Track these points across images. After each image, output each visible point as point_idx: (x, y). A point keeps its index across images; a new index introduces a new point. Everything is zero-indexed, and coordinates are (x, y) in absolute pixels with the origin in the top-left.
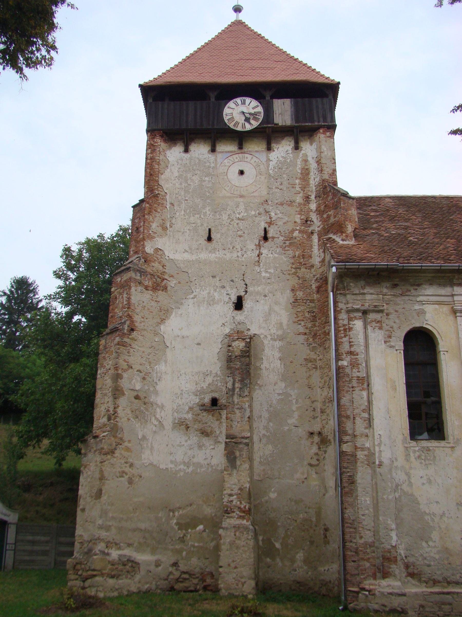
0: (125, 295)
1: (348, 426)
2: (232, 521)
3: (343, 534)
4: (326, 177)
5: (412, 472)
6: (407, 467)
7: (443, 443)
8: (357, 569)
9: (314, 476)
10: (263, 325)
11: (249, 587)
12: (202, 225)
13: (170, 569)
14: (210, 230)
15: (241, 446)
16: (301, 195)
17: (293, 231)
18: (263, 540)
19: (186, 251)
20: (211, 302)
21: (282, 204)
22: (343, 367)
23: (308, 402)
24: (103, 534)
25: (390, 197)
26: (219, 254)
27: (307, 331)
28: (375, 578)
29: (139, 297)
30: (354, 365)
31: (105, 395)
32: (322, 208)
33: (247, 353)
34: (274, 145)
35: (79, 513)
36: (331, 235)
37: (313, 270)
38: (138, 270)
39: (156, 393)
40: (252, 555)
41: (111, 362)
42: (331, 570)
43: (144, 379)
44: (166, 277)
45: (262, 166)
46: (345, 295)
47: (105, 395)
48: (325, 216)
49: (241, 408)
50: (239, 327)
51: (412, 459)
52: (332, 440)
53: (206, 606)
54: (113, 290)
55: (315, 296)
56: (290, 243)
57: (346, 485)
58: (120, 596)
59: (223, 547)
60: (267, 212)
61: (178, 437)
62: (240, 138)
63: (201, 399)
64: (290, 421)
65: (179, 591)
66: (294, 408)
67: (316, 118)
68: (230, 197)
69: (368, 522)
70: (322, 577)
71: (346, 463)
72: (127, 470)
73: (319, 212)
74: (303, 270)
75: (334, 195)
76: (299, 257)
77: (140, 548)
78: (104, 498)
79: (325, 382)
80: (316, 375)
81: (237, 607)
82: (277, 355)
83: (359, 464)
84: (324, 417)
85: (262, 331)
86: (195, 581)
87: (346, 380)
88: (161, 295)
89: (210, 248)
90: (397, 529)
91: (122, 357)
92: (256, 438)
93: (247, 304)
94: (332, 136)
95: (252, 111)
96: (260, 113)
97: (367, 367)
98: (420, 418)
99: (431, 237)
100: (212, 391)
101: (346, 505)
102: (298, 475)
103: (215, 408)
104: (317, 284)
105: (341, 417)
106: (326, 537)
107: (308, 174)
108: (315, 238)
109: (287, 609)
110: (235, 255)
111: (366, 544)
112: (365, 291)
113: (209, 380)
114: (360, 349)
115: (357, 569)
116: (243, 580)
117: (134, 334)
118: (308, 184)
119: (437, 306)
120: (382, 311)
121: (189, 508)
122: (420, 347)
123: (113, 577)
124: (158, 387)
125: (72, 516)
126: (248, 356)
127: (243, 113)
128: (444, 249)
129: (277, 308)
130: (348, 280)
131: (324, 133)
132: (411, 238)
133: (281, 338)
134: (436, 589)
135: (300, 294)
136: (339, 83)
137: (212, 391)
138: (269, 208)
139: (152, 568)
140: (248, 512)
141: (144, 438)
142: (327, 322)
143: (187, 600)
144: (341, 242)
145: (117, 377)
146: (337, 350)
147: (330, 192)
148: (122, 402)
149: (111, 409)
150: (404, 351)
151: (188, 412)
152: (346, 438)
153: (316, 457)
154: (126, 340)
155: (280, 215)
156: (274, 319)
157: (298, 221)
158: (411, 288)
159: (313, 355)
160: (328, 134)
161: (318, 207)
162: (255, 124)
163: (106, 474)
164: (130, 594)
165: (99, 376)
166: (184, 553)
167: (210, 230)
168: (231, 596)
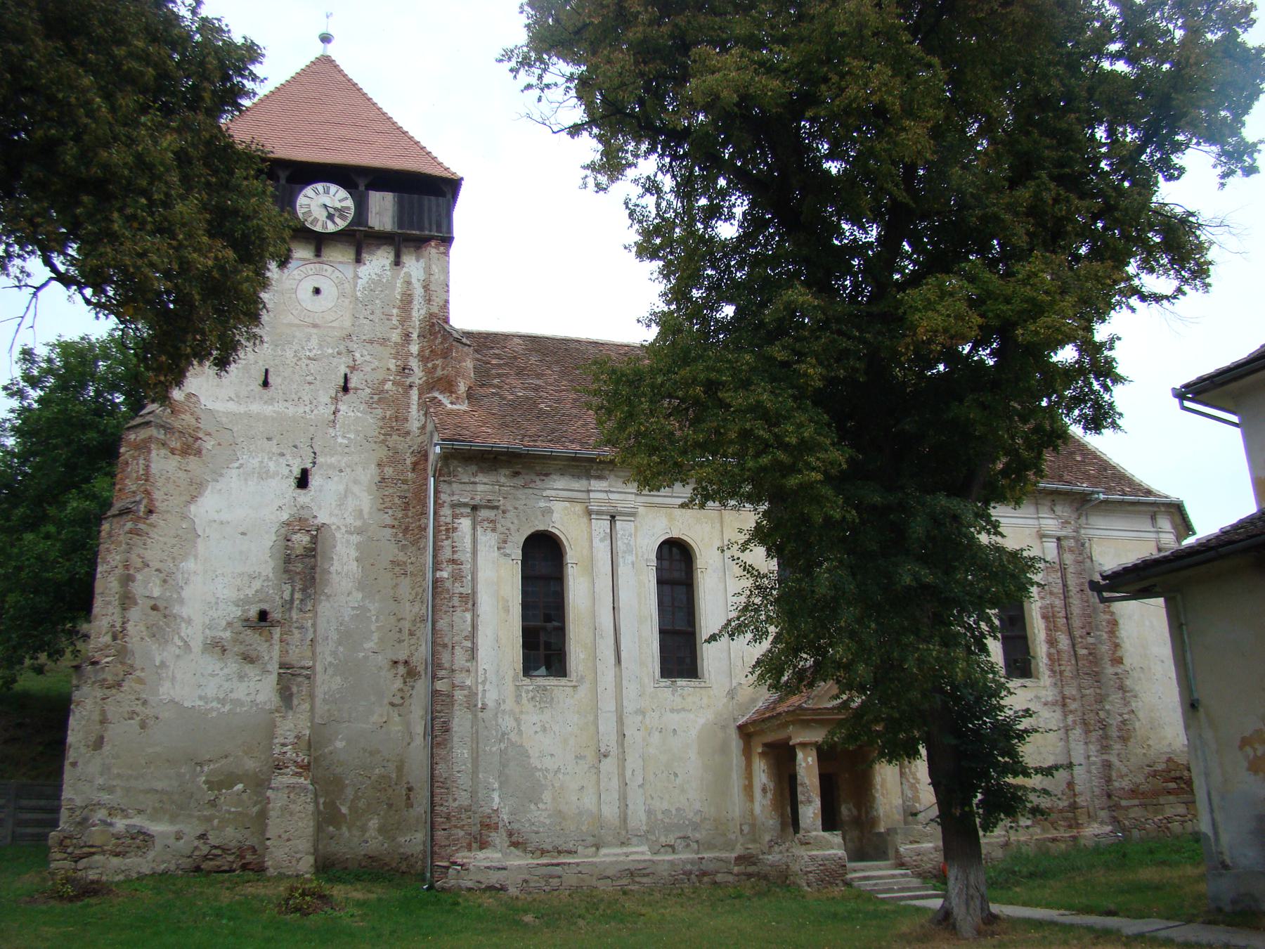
0: (141, 462)
1: (445, 658)
2: (281, 780)
3: (432, 796)
4: (435, 310)
5: (523, 717)
6: (517, 710)
7: (563, 681)
8: (447, 839)
9: (397, 719)
10: (336, 512)
11: (306, 865)
12: (256, 362)
13: (196, 843)
14: (267, 371)
15: (300, 679)
16: (399, 331)
17: (384, 381)
18: (324, 803)
19: (231, 399)
20: (264, 475)
21: (371, 342)
22: (442, 580)
23: (392, 619)
24: (105, 797)
25: (520, 336)
26: (279, 407)
27: (396, 523)
28: (470, 850)
29: (162, 464)
30: (457, 577)
31: (109, 603)
32: (427, 353)
33: (311, 552)
34: (365, 256)
35: (67, 767)
36: (436, 394)
37: (408, 438)
38: (162, 426)
39: (181, 601)
40: (312, 824)
41: (118, 557)
42: (414, 841)
43: (165, 581)
44: (200, 435)
45: (346, 285)
46: (450, 483)
47: (109, 603)
48: (430, 365)
49: (301, 628)
50: (301, 512)
51: (524, 701)
52: (423, 673)
53: (250, 890)
54: (122, 450)
55: (410, 475)
56: (380, 400)
57: (438, 733)
58: (128, 880)
59: (272, 813)
60: (349, 351)
61: (211, 664)
62: (319, 242)
63: (244, 611)
64: (367, 646)
65: (209, 872)
66: (373, 628)
67: (426, 225)
68: (298, 326)
69: (464, 780)
70: (402, 850)
71: (439, 706)
72: (138, 709)
73: (423, 358)
74: (395, 437)
75: (445, 339)
76: (390, 418)
77: (155, 815)
78: (106, 748)
79: (417, 594)
80: (405, 585)
81: (297, 889)
82: (354, 554)
83: (456, 707)
84: (412, 642)
85: (333, 520)
86: (231, 858)
87: (444, 596)
88: (193, 462)
89: (266, 397)
90: (500, 788)
91: (136, 550)
92: (319, 668)
93: (314, 481)
94: (446, 254)
95: (338, 205)
96: (348, 208)
97: (474, 580)
98: (536, 648)
99: (568, 406)
100: (260, 601)
101: (437, 759)
102: (375, 718)
103: (263, 624)
104: (414, 459)
105: (437, 645)
106: (409, 798)
107: (411, 302)
108: (414, 393)
109: (356, 890)
110: (301, 410)
111: (460, 808)
112: (477, 480)
113: (257, 585)
114: (466, 556)
115: (447, 839)
116: (298, 856)
117: (153, 517)
118: (409, 317)
119: (567, 504)
120: (496, 508)
121: (223, 761)
122: (543, 558)
123: (117, 855)
124: (185, 594)
125: (56, 774)
126: (314, 556)
127: (325, 206)
128: (583, 426)
129: (356, 489)
130: (456, 463)
131: (437, 247)
132: (542, 406)
133: (360, 532)
134: (544, 861)
135: (389, 471)
136: (462, 179)
137: (260, 601)
138: (353, 346)
139: (171, 841)
140: (306, 767)
141: (163, 665)
142: (424, 513)
143: (223, 882)
144: (449, 406)
145: (127, 579)
146: (435, 556)
147: (438, 332)
148: (134, 614)
149: (118, 625)
150: (522, 562)
151: (225, 629)
152: (441, 673)
153: (400, 694)
154: (141, 526)
155: (368, 358)
156: (351, 503)
157: (393, 367)
158: (537, 479)
159: (401, 557)
160: (442, 249)
161: (421, 350)
162: (342, 224)
163: (109, 716)
164: (141, 877)
165: (98, 576)
166: (216, 822)
167: (267, 371)
168: (281, 877)
